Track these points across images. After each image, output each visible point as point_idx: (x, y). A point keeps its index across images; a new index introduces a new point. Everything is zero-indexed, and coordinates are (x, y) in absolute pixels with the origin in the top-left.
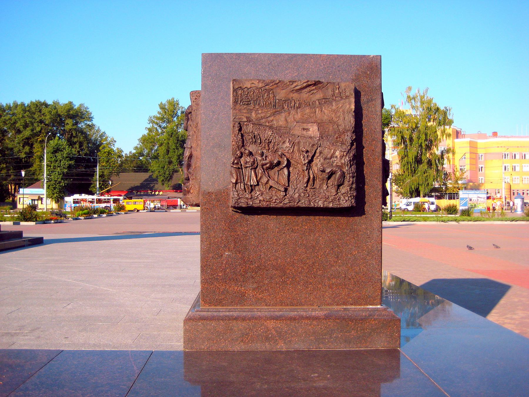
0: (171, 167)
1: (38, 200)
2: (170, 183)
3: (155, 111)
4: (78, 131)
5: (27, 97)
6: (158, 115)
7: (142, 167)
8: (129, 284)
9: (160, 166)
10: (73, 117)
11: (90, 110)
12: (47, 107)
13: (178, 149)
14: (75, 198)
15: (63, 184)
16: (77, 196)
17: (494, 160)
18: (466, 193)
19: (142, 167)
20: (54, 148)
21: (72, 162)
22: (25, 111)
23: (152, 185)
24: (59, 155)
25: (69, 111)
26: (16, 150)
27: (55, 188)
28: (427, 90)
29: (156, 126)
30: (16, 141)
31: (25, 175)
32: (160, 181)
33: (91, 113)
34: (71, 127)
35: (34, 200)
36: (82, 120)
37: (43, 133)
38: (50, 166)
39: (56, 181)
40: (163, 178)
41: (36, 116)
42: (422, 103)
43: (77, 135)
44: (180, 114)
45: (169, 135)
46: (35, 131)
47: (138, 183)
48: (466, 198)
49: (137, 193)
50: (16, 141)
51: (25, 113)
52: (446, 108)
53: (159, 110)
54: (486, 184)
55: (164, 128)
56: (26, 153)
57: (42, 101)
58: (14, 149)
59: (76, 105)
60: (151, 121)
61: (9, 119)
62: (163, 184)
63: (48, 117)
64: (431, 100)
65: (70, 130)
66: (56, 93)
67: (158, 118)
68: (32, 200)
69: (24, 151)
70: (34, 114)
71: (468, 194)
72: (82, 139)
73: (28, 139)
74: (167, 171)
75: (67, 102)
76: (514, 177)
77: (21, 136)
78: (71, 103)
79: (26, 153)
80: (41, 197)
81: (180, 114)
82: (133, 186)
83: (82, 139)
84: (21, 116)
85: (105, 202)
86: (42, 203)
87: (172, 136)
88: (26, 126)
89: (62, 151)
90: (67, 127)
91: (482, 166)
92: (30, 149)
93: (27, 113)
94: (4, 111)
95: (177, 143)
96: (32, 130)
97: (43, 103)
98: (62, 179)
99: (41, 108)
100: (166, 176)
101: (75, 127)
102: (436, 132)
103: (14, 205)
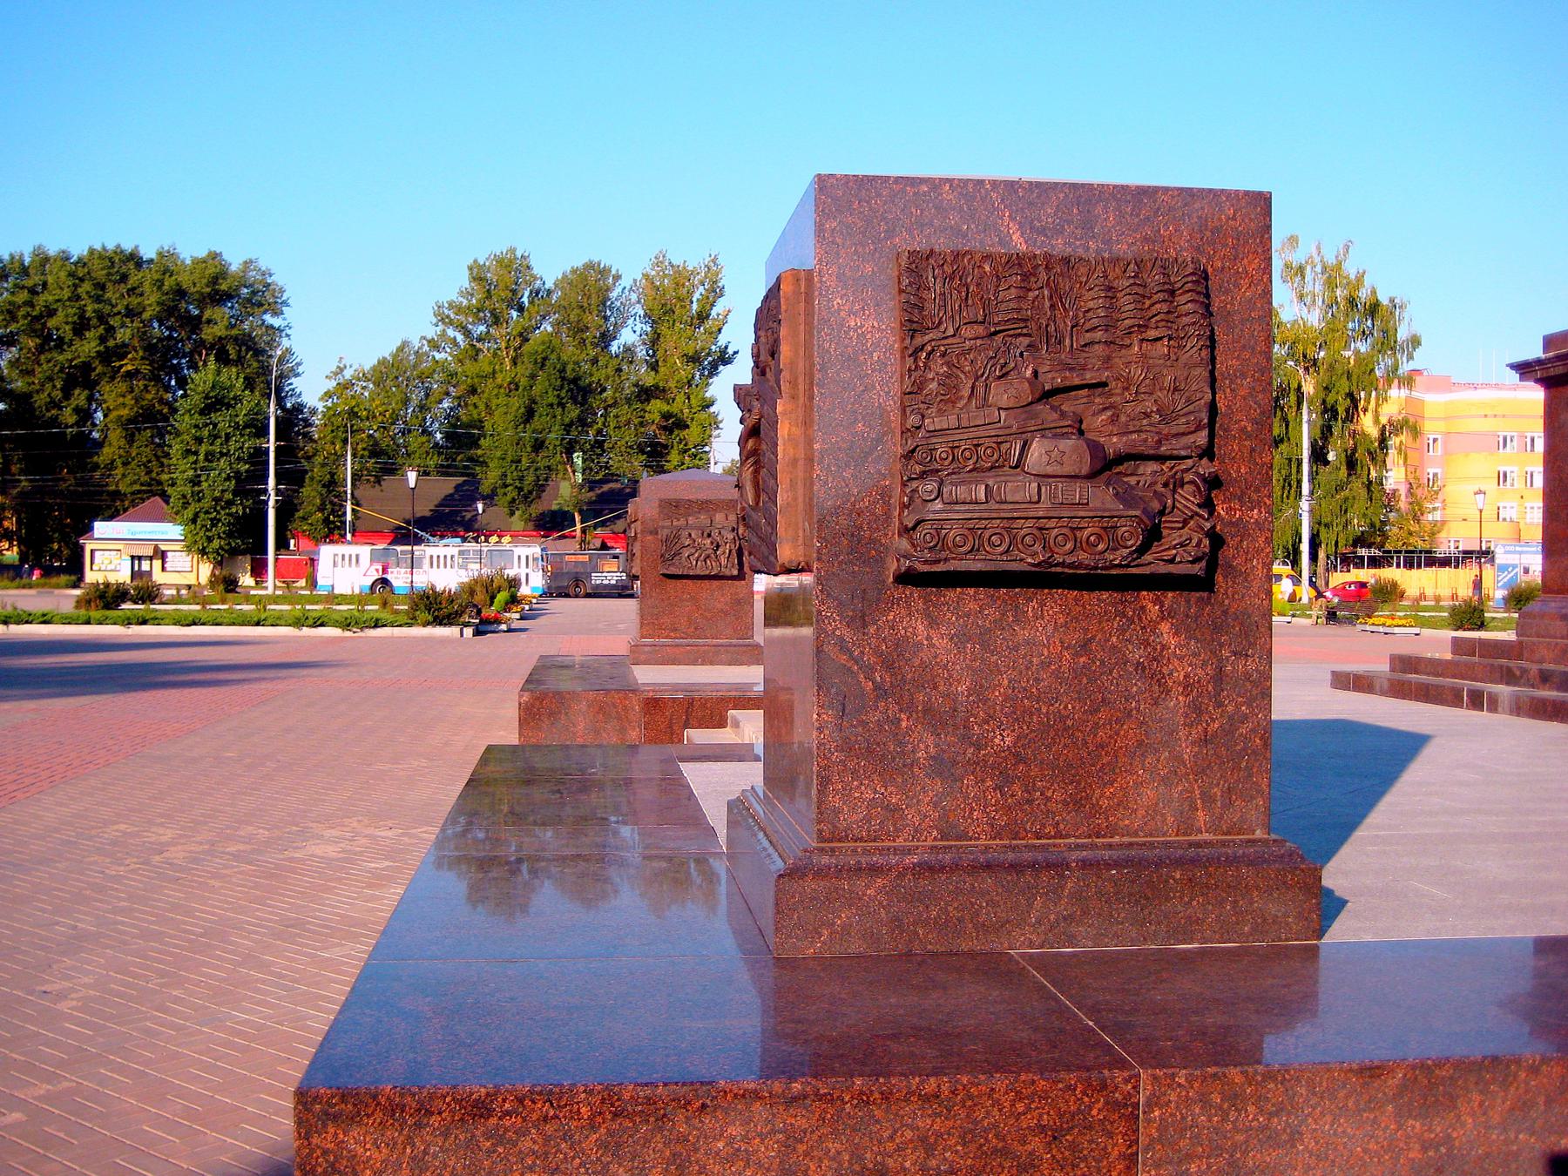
1: (151, 558)
3: (454, 285)
8: (300, 794)
11: (278, 279)
13: (562, 405)
15: (237, 509)
17: (1474, 456)
18: (1515, 552)
20: (207, 397)
23: (468, 516)
24: (222, 419)
25: (215, 280)
26: (40, 400)
28: (1347, 248)
29: (451, 332)
30: (41, 372)
33: (282, 291)
34: (223, 333)
35: (140, 558)
38: (196, 453)
39: (217, 500)
40: (515, 494)
42: (1330, 284)
44: (525, 299)
46: (111, 343)
48: (1515, 566)
50: (41, 372)
52: (1392, 300)
54: (1453, 525)
55: (479, 340)
57: (128, 247)
60: (443, 319)
62: (512, 514)
64: (1360, 278)
67: (459, 309)
68: (133, 557)
69: (74, 403)
70: (103, 287)
71: (1521, 553)
73: (86, 367)
75: (202, 253)
76: (1528, 505)
78: (214, 256)
80: (163, 548)
84: (66, 294)
86: (163, 569)
87: (543, 365)
88: (81, 327)
89: (229, 406)
91: (1438, 470)
93: (86, 287)
95: (562, 387)
96: (103, 340)
98: (235, 493)
102: (1372, 370)
103: (75, 567)
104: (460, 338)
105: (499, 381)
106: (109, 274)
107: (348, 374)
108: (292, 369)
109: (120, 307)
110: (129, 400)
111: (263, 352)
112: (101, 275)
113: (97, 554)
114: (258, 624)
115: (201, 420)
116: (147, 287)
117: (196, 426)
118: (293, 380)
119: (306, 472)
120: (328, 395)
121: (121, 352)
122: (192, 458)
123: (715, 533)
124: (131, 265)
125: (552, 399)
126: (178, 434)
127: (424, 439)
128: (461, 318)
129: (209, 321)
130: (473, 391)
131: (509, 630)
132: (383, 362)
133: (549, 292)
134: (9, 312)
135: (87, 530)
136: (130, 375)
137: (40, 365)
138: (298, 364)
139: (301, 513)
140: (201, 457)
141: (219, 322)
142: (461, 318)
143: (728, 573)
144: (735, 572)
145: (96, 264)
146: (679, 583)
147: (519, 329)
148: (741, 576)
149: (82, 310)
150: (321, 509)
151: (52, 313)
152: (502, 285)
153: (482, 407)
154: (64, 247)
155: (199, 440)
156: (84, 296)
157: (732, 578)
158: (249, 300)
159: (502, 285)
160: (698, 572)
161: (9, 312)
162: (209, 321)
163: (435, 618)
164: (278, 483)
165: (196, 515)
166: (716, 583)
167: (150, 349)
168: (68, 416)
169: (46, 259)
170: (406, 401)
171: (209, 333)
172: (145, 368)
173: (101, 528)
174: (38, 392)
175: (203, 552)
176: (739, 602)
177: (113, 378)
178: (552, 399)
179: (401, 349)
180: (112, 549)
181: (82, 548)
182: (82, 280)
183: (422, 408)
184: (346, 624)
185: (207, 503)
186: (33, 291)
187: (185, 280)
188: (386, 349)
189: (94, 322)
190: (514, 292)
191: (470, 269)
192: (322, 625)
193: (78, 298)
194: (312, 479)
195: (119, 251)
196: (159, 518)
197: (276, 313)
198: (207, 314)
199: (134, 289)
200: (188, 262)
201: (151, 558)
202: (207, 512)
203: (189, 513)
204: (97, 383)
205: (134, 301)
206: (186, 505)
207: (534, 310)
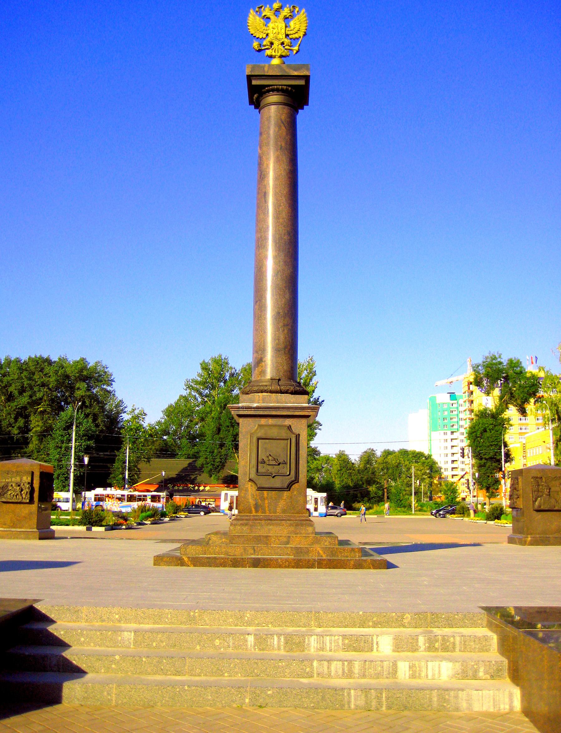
0: (223, 451)
2: (218, 475)
3: (194, 372)
4: (93, 398)
5: (24, 354)
6: (199, 379)
7: (167, 450)
9: (208, 450)
10: (85, 379)
11: (110, 370)
12: (51, 365)
14: (97, 493)
16: (99, 491)
19: (167, 450)
20: (67, 423)
21: (91, 443)
23: (193, 477)
25: (81, 370)
31: (89, 461)
32: (206, 470)
33: (111, 375)
34: (84, 394)
36: (99, 384)
37: (45, 401)
38: (61, 448)
40: (211, 467)
41: (36, 377)
43: (91, 405)
44: (227, 378)
45: (221, 407)
46: (34, 398)
47: (173, 474)
49: (173, 487)
51: (21, 373)
53: (200, 371)
56: (19, 428)
57: (45, 356)
59: (91, 363)
60: (189, 387)
62: (211, 476)
63: (53, 379)
65: (82, 396)
66: (63, 344)
67: (197, 382)
69: (17, 425)
70: (34, 374)
72: (97, 410)
73: (25, 408)
74: (218, 457)
77: (16, 404)
78: (83, 360)
79: (19, 428)
81: (227, 378)
83: (97, 410)
84: (16, 377)
85: (140, 500)
87: (225, 408)
88: (22, 391)
90: (78, 394)
93: (25, 373)
96: (31, 397)
99: (43, 366)
100: (217, 464)
101: (88, 393)
106: (35, 368)
107: (137, 412)
108: (122, 410)
110: (41, 424)
111: (102, 402)
112: (32, 368)
115: (63, 433)
116: (51, 374)
117: (62, 436)
118: (122, 415)
119: (116, 456)
121: (38, 402)
122: (59, 450)
124: (46, 364)
125: (228, 424)
126: (54, 439)
128: (198, 387)
129: (78, 388)
132: (170, 406)
136: (42, 413)
137: (5, 407)
139: (112, 475)
140: (63, 449)
141: (81, 389)
142: (198, 387)
143: (24, 501)
145: (30, 364)
149: (22, 383)
151: (11, 385)
155: (62, 442)
156: (24, 378)
160: (13, 501)
162: (78, 388)
167: (52, 400)
168: (15, 431)
169: (10, 361)
170: (181, 425)
171: (78, 394)
172: (49, 410)
177: (35, 413)
178: (228, 424)
183: (188, 427)
187: (69, 371)
189: (28, 389)
191: (201, 364)
195: (41, 358)
198: (77, 385)
202: (64, 474)
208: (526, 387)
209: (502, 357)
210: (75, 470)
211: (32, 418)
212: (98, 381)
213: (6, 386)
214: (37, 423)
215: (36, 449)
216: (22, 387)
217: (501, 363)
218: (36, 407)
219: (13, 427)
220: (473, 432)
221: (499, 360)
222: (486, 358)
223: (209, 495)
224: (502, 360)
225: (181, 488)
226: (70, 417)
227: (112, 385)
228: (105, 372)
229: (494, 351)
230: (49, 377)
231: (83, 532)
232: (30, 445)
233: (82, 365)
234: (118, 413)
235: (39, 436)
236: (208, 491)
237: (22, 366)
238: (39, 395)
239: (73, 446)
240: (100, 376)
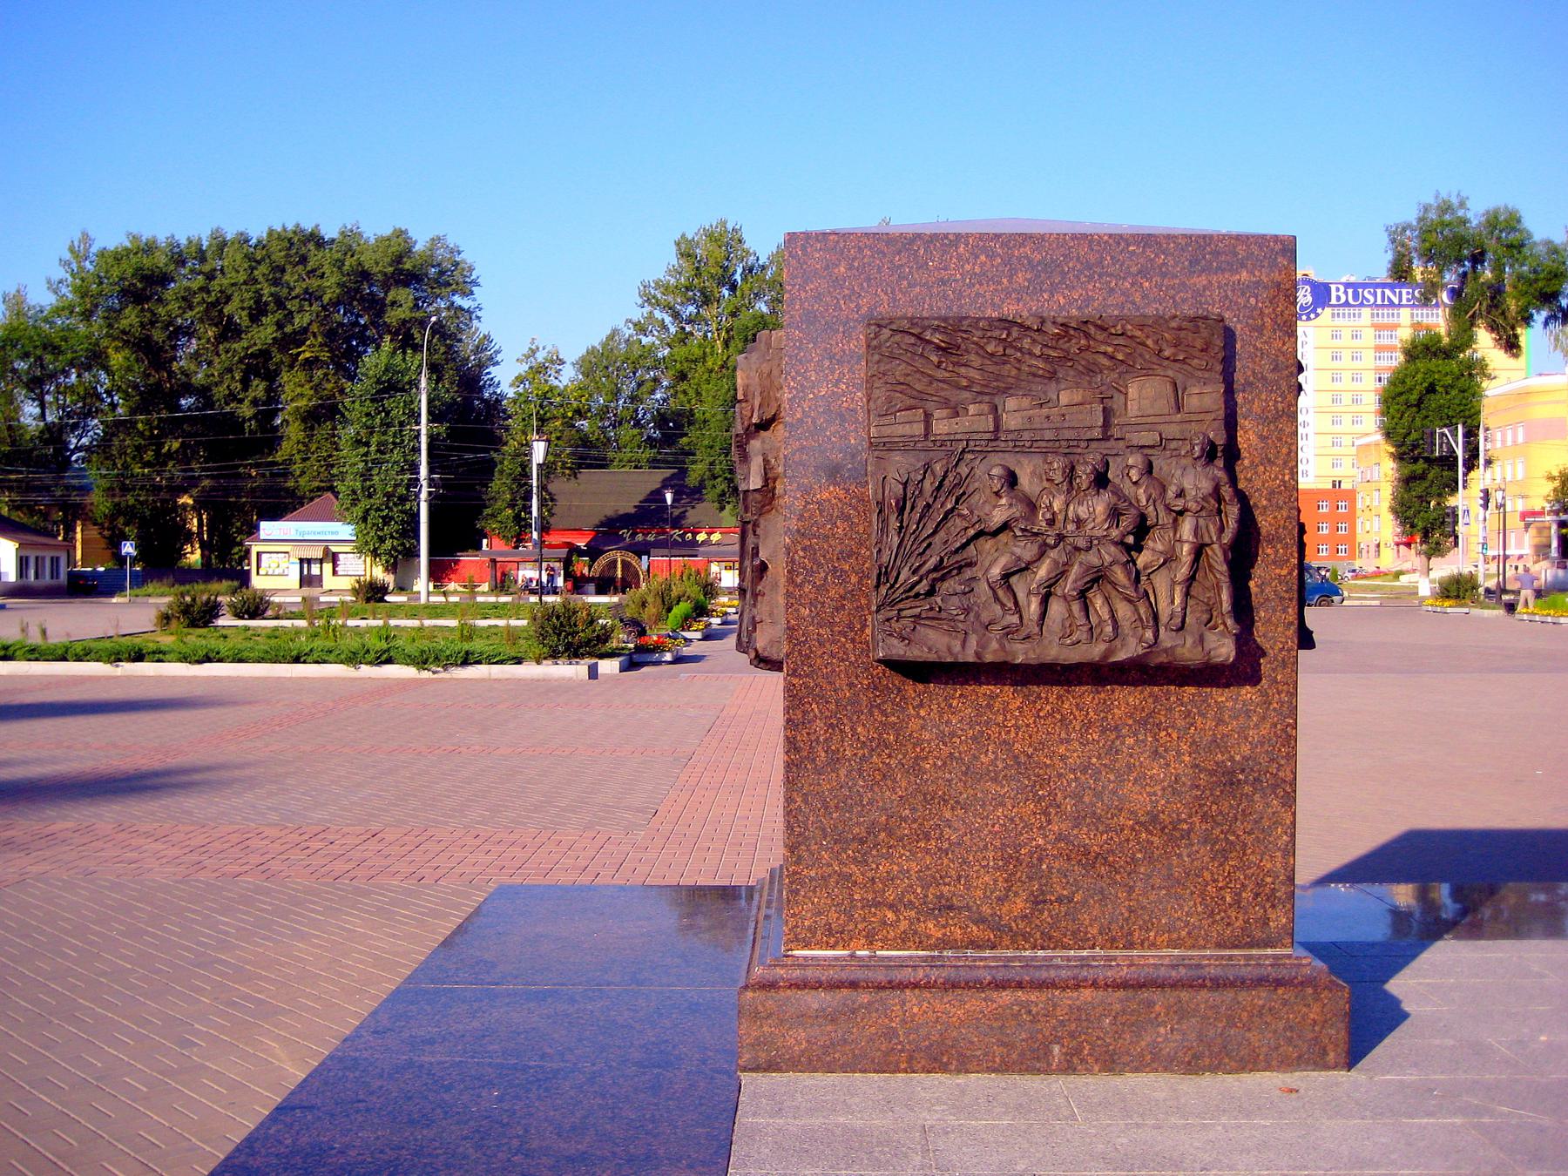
1: (321, 561)
3: (661, 263)
5: (256, 214)
6: (673, 281)
10: (410, 278)
11: (467, 257)
20: (379, 382)
22: (253, 261)
25: (399, 259)
26: (220, 392)
27: (387, 520)
29: (658, 314)
31: (674, 501)
32: (710, 495)
33: (471, 269)
35: (309, 561)
37: (315, 335)
38: (367, 444)
39: (389, 496)
40: (724, 486)
44: (738, 277)
47: (628, 506)
49: (633, 535)
53: (673, 260)
55: (690, 321)
56: (255, 402)
57: (308, 226)
58: (215, 390)
60: (649, 300)
61: (201, 289)
62: (722, 508)
65: (404, 322)
66: (352, 195)
67: (666, 289)
68: (301, 561)
69: (251, 394)
70: (283, 271)
73: (265, 354)
78: (400, 233)
79: (255, 402)
80: (334, 549)
82: (610, 513)
84: (242, 277)
86: (335, 573)
88: (258, 312)
89: (403, 390)
90: (393, 316)
92: (268, 390)
93: (263, 269)
94: (181, 262)
96: (280, 325)
97: (312, 235)
99: (304, 250)
104: (668, 320)
105: (710, 364)
106: (287, 256)
107: (540, 356)
108: (491, 358)
109: (297, 291)
111: (453, 336)
112: (279, 257)
113: (264, 557)
114: (297, 660)
116: (326, 269)
117: (368, 415)
118: (491, 369)
120: (520, 380)
121: (298, 338)
122: (363, 450)
123: (1126, 469)
124: (311, 246)
127: (636, 431)
130: (683, 376)
131: (678, 660)
132: (592, 351)
133: (763, 268)
134: (184, 299)
135: (253, 530)
136: (310, 364)
137: (218, 355)
138: (498, 352)
139: (488, 511)
140: (373, 448)
142: (670, 299)
143: (1187, 651)
144: (1224, 649)
145: (275, 246)
146: (964, 702)
147: (731, 308)
148: (1246, 668)
150: (512, 505)
151: (228, 299)
152: (712, 261)
153: (692, 393)
154: (241, 229)
156: (261, 279)
157: (1209, 675)
158: (436, 281)
159: (712, 261)
160: (1053, 651)
161: (184, 299)
162: (393, 303)
163: (568, 646)
164: (431, 471)
165: (367, 512)
166: (1127, 698)
167: (331, 335)
168: (246, 410)
169: (224, 244)
170: (616, 393)
171: (393, 316)
172: (325, 355)
173: (268, 528)
174: (216, 384)
175: (375, 554)
176: (1229, 780)
177: (291, 367)
179: (611, 337)
180: (278, 554)
181: (248, 552)
182: (259, 262)
183: (633, 399)
184: (422, 662)
185: (378, 499)
186: (210, 277)
188: (596, 338)
190: (725, 269)
191: (678, 244)
192: (389, 661)
193: (256, 281)
194: (501, 472)
196: (329, 518)
197: (468, 294)
199: (313, 271)
200: (372, 241)
201: (321, 561)
203: (358, 511)
204: (277, 373)
205: (314, 283)
206: (355, 502)
207: (746, 287)
208: (1536, 280)
209: (1469, 204)
210: (430, 493)
211: (285, 377)
212: (440, 285)
213: (218, 302)
214: (299, 390)
215: (299, 451)
216: (258, 302)
217: (1464, 222)
218: (294, 351)
219: (241, 401)
220: (1401, 394)
221: (1460, 213)
222: (1426, 209)
223: (717, 554)
224: (1470, 215)
225: (651, 538)
226: (387, 370)
227: (472, 293)
228: (456, 264)
229: (1449, 190)
230: (322, 276)
231: (581, 684)
232: (284, 444)
233: (399, 246)
234: (481, 366)
235: (304, 420)
236: (718, 544)
237: (255, 255)
238: (300, 321)
239: (424, 431)
240: (442, 273)
